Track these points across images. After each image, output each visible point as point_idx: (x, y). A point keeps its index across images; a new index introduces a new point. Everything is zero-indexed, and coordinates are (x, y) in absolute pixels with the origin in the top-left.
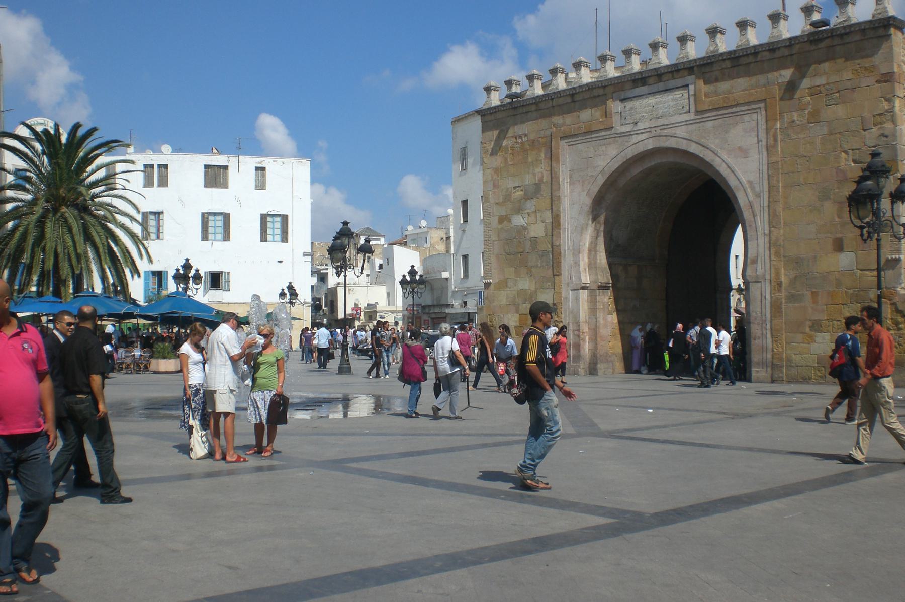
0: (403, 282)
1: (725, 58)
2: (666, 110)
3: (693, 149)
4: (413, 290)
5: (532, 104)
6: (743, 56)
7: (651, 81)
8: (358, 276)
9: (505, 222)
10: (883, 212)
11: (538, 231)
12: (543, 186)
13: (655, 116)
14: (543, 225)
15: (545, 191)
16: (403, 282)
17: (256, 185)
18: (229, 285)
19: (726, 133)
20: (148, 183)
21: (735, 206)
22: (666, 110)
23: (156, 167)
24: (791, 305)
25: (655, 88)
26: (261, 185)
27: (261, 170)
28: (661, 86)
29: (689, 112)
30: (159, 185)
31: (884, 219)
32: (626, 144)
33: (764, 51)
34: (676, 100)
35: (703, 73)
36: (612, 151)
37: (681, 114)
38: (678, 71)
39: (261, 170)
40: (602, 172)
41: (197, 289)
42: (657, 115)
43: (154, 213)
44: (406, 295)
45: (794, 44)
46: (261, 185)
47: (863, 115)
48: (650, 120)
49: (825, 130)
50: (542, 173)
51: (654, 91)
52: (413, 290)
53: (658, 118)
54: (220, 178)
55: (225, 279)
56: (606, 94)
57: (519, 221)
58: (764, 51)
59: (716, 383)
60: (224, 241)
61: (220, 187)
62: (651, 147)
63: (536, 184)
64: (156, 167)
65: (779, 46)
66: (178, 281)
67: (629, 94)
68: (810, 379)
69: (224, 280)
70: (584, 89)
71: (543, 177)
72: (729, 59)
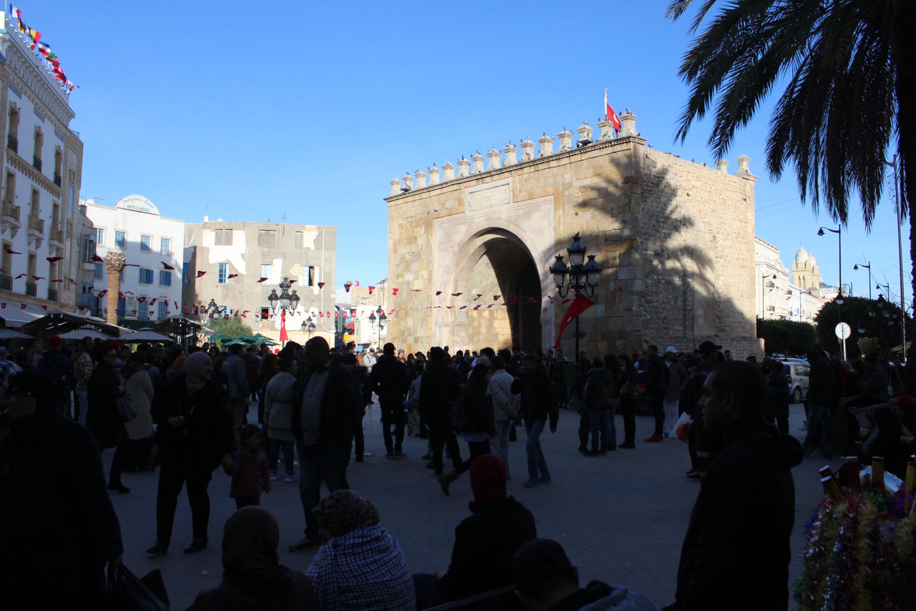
29: (509, 203)
53: (491, 207)
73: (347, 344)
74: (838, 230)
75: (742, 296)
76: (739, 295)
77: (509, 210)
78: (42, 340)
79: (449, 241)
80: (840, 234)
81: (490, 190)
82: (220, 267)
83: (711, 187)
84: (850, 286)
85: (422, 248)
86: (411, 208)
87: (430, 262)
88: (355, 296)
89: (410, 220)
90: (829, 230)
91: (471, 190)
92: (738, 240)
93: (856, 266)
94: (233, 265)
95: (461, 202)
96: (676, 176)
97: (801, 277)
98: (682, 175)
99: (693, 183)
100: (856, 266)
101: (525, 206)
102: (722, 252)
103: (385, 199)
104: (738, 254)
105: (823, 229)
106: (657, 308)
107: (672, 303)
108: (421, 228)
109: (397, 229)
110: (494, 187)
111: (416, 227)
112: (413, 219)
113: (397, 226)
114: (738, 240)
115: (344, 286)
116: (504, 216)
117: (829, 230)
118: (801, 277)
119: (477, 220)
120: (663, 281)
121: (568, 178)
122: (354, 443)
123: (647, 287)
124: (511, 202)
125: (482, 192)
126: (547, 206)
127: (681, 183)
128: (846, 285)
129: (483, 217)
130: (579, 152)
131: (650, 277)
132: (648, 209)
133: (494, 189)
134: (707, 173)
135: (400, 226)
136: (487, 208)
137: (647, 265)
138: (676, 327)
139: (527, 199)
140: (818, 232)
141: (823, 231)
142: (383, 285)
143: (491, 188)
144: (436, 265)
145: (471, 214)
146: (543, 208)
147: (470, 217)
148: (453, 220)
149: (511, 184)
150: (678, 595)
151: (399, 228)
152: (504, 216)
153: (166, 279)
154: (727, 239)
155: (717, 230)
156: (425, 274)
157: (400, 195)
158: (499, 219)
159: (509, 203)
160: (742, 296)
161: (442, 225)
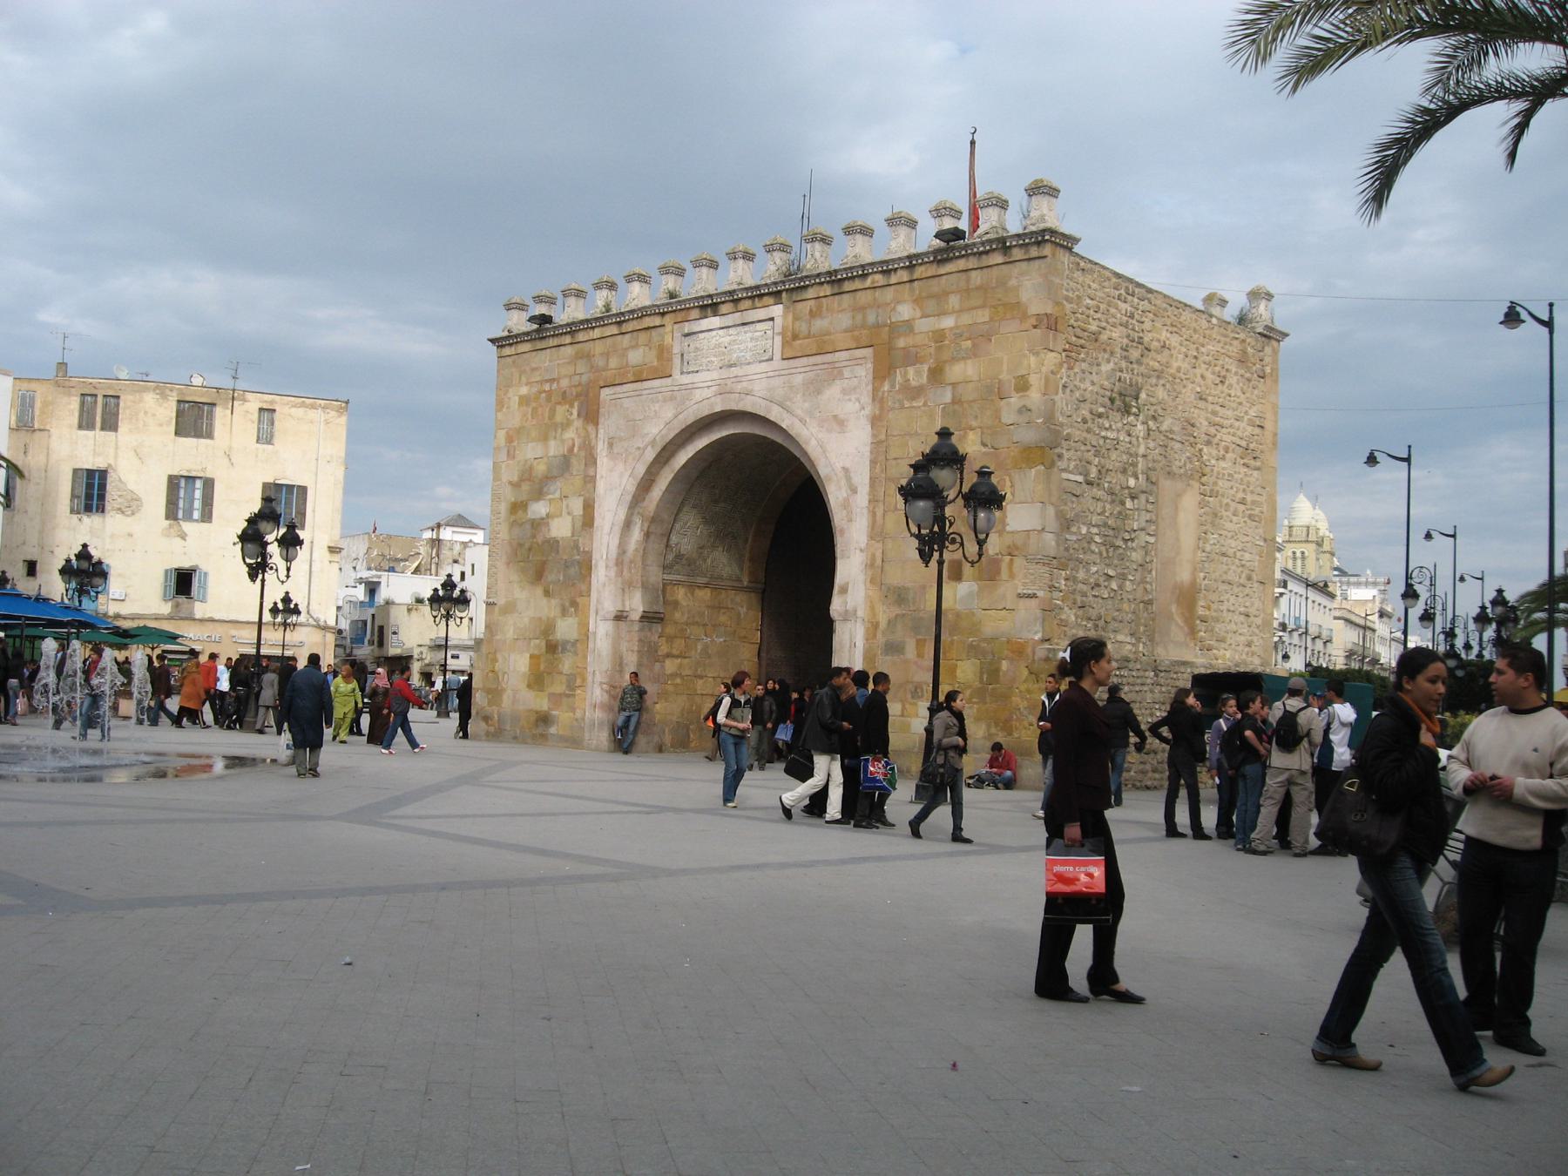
0: (63, 572)
1: (823, 280)
2: (743, 354)
3: (775, 414)
4: (448, 613)
5: (565, 333)
6: (848, 279)
7: (724, 309)
8: (283, 582)
9: (520, 512)
10: (950, 521)
11: (561, 529)
12: (574, 461)
13: (727, 363)
14: (570, 518)
15: (577, 466)
16: (63, 572)
17: (258, 437)
18: (205, 592)
19: (818, 394)
20: (86, 423)
21: (828, 505)
22: (743, 354)
23: (100, 399)
24: (888, 658)
25: (729, 320)
26: (266, 436)
27: (267, 412)
29: (772, 359)
30: (102, 429)
31: (951, 531)
32: (687, 402)
33: (876, 272)
34: (757, 340)
35: (795, 302)
36: (668, 413)
37: (760, 362)
38: (761, 296)
39: (267, 412)
40: (653, 443)
41: (461, 618)
42: (729, 361)
43: (187, 478)
44: (438, 619)
45: (915, 265)
46: (266, 436)
47: (1000, 377)
48: (721, 368)
49: (948, 397)
50: (573, 440)
51: (727, 324)
52: (448, 613)
53: (731, 366)
54: (202, 423)
55: (200, 583)
56: (664, 325)
57: (539, 509)
58: (876, 272)
59: (21, 704)
60: (203, 521)
61: (198, 435)
62: (719, 410)
63: (564, 456)
64: (100, 399)
65: (896, 266)
66: (67, 577)
67: (696, 327)
68: (908, 771)
69: (197, 585)
70: (636, 316)
71: (574, 445)
72: (828, 282)
73: (103, 650)
74: (1406, 456)
75: (1249, 578)
76: (1244, 576)
78: (1021, 279)
80: (1409, 465)
81: (731, 331)
82: (87, 479)
83: (1197, 349)
84: (1433, 574)
85: (571, 450)
86: (555, 362)
87: (590, 480)
88: (375, 553)
89: (547, 387)
90: (1389, 455)
92: (1245, 461)
93: (1428, 532)
95: (663, 353)
96: (1131, 321)
97: (1298, 555)
98: (1144, 319)
99: (1164, 335)
101: (808, 369)
102: (1215, 484)
103: (493, 341)
104: (1244, 490)
105: (1376, 454)
106: (1084, 595)
107: (1114, 586)
108: (572, 406)
109: (517, 406)
110: (738, 325)
111: (559, 403)
113: (517, 398)
114: (1245, 461)
116: (759, 387)
117: (1389, 455)
118: (1298, 555)
119: (698, 395)
120: (1097, 539)
121: (905, 311)
123: (1067, 549)
124: (778, 356)
125: (714, 333)
127: (1141, 335)
128: (1424, 570)
129: (714, 389)
131: (1074, 529)
132: (1075, 386)
134: (1191, 319)
135: (524, 400)
136: (721, 368)
137: (1069, 504)
138: (1120, 637)
139: (814, 352)
140: (1365, 460)
141: (1375, 458)
142: (438, 534)
143: (734, 326)
144: (601, 486)
145: (686, 379)
147: (683, 387)
148: (645, 392)
149: (778, 321)
151: (520, 404)
152: (759, 387)
153: (1254, 41)
154: (1223, 458)
155: (1206, 438)
156: (577, 506)
157: (527, 334)
159: (772, 359)
160: (1249, 578)
161: (614, 401)
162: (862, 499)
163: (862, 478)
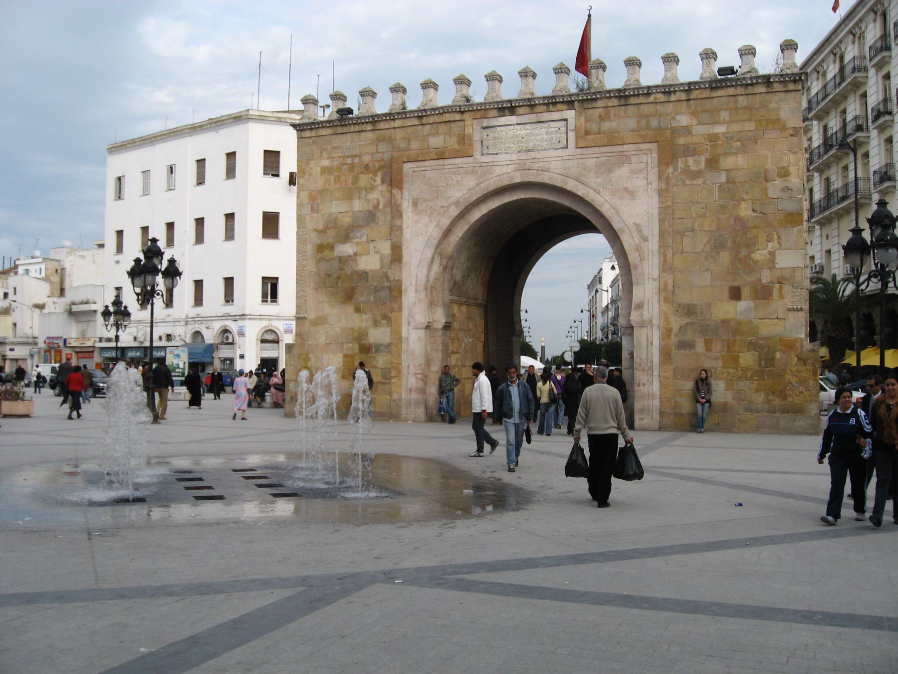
28: (533, 117)
29: (567, 147)
53: (529, 151)
77: (564, 158)
79: (437, 198)
91: (485, 123)
93: (613, 266)
94: (142, 186)
100: (613, 266)
101: (599, 155)
110: (534, 123)
112: (357, 160)
113: (319, 169)
115: (126, 273)
119: (498, 170)
122: (588, 464)
126: (644, 158)
130: (404, 116)
133: (534, 125)
146: (634, 159)
150: (885, 502)
158: (547, 170)
162: (653, 244)
163: (653, 231)
